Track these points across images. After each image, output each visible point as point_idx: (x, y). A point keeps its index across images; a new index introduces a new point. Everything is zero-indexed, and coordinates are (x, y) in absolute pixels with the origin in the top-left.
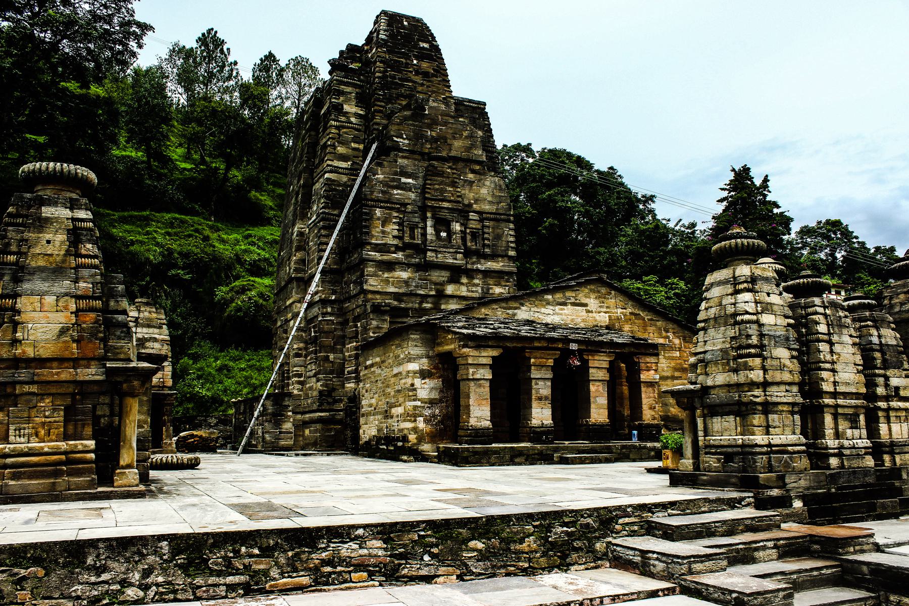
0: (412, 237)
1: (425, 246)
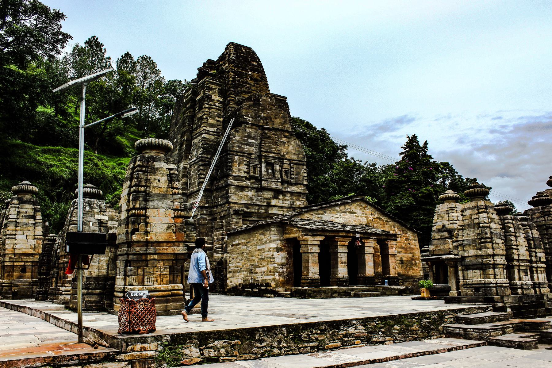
0: (254, 173)
1: (261, 177)
